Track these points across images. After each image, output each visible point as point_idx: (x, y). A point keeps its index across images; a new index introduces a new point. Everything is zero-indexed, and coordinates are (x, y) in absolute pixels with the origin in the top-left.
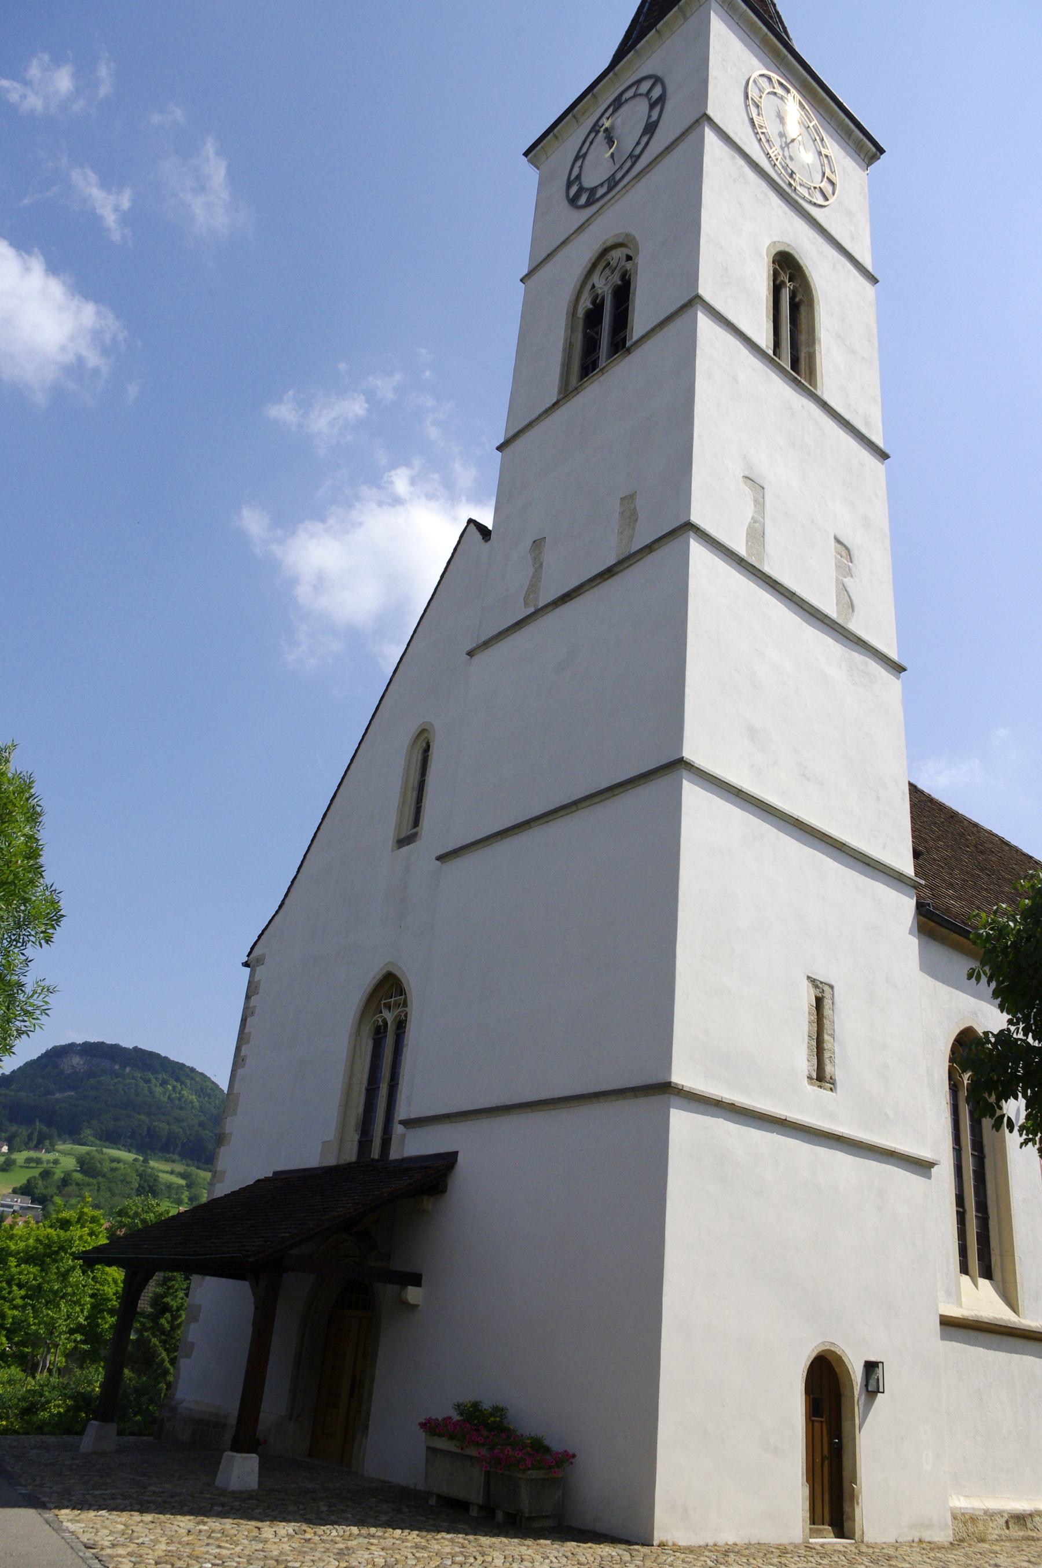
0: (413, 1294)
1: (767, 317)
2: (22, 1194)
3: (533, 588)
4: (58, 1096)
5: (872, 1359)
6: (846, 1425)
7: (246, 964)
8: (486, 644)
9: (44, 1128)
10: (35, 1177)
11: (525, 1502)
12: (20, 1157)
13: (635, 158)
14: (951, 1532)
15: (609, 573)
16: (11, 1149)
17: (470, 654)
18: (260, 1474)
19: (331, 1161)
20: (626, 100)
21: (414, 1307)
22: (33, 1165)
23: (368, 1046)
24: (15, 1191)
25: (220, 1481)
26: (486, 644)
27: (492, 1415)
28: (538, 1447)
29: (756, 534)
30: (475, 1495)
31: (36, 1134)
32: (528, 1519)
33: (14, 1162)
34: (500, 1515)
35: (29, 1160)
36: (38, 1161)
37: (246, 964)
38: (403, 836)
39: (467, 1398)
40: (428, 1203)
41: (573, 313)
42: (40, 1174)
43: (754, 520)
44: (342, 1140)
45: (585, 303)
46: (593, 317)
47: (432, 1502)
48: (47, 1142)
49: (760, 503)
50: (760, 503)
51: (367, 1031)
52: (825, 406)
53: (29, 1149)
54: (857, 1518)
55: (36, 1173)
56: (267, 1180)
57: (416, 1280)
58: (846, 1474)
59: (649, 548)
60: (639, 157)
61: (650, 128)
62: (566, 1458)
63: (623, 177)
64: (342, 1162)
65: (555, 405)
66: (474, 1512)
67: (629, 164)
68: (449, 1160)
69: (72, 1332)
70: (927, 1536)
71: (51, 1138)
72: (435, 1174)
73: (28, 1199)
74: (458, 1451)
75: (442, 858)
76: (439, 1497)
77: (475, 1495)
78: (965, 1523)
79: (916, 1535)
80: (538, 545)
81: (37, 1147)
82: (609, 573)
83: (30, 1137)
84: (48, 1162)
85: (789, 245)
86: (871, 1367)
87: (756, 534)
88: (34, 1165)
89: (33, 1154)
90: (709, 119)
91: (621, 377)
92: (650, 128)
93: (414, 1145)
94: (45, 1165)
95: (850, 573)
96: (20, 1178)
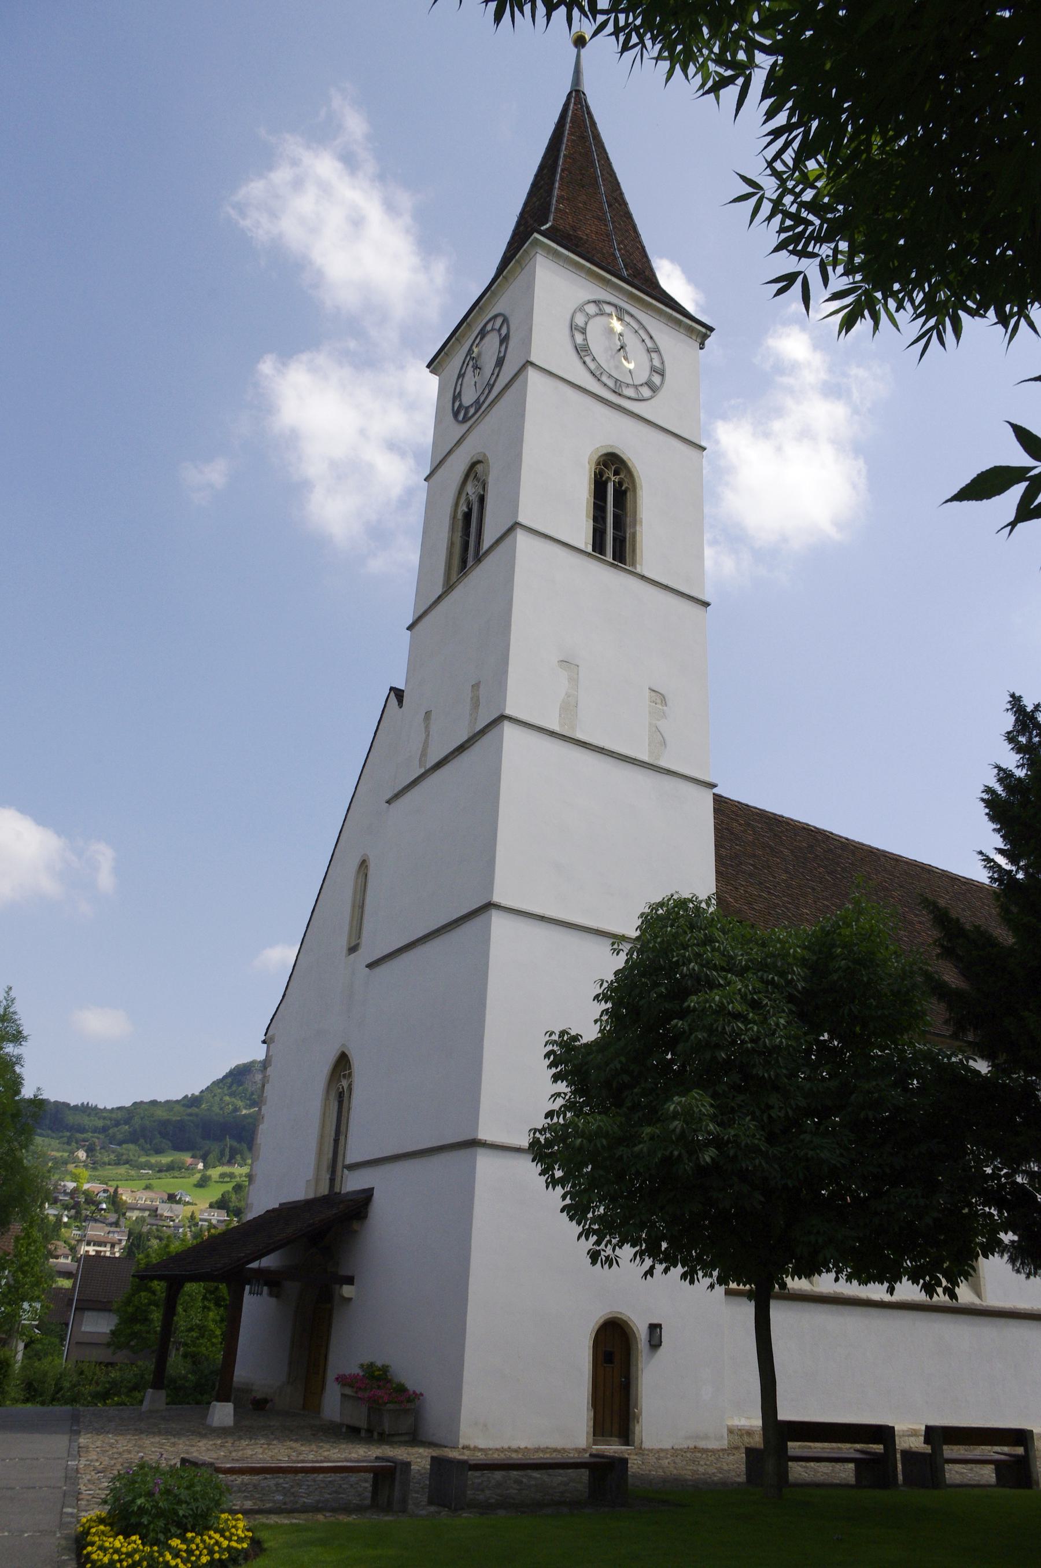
0: (347, 1291)
1: (587, 516)
2: (219, 1208)
3: (424, 754)
4: (244, 1112)
5: (655, 1322)
6: (633, 1369)
7: (264, 1042)
8: (397, 796)
9: (235, 1144)
10: (228, 1192)
11: (386, 1428)
12: (215, 1173)
13: (491, 386)
14: (726, 1442)
15: (461, 749)
16: (206, 1167)
17: (388, 802)
18: (235, 1415)
19: (311, 1196)
20: (488, 332)
21: (350, 1299)
22: (226, 1179)
23: (334, 1106)
24: (211, 1206)
25: (208, 1421)
26: (397, 796)
27: (379, 1370)
28: (402, 1389)
29: (569, 708)
30: (363, 1424)
31: (227, 1150)
32: (389, 1435)
33: (209, 1178)
34: (375, 1435)
35: (223, 1175)
36: (231, 1176)
37: (264, 1042)
38: (352, 945)
39: (366, 1360)
40: (355, 1225)
41: (454, 517)
42: (234, 1188)
43: (568, 695)
44: (317, 1180)
45: (464, 508)
46: (467, 516)
47: (344, 1430)
48: (238, 1157)
49: (574, 681)
50: (574, 681)
51: (333, 1095)
52: (643, 577)
53: (223, 1164)
54: (637, 1432)
55: (229, 1187)
56: (274, 1210)
57: (350, 1280)
58: (632, 1403)
59: (483, 732)
60: (493, 385)
61: (500, 362)
62: (417, 1396)
63: (484, 402)
64: (319, 1195)
65: (440, 598)
66: (363, 1434)
67: (486, 392)
68: (366, 1197)
69: (191, 1330)
70: (702, 1444)
71: (241, 1153)
72: (360, 1205)
73: (224, 1213)
74: (353, 1394)
75: (371, 966)
76: (348, 1427)
77: (363, 1424)
78: (741, 1436)
79: (691, 1444)
80: (428, 714)
81: (230, 1162)
82: (461, 749)
83: (222, 1154)
84: (241, 1176)
85: (611, 446)
86: (655, 1329)
87: (569, 708)
88: (226, 1179)
89: (226, 1169)
90: (532, 364)
91: (480, 576)
92: (500, 362)
93: (353, 1183)
94: (238, 1179)
95: (664, 715)
96: (215, 1193)
